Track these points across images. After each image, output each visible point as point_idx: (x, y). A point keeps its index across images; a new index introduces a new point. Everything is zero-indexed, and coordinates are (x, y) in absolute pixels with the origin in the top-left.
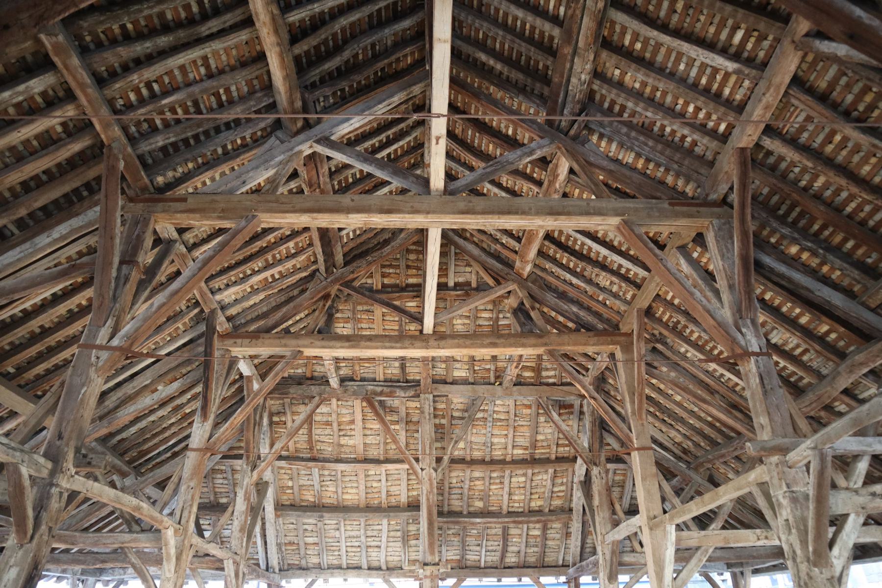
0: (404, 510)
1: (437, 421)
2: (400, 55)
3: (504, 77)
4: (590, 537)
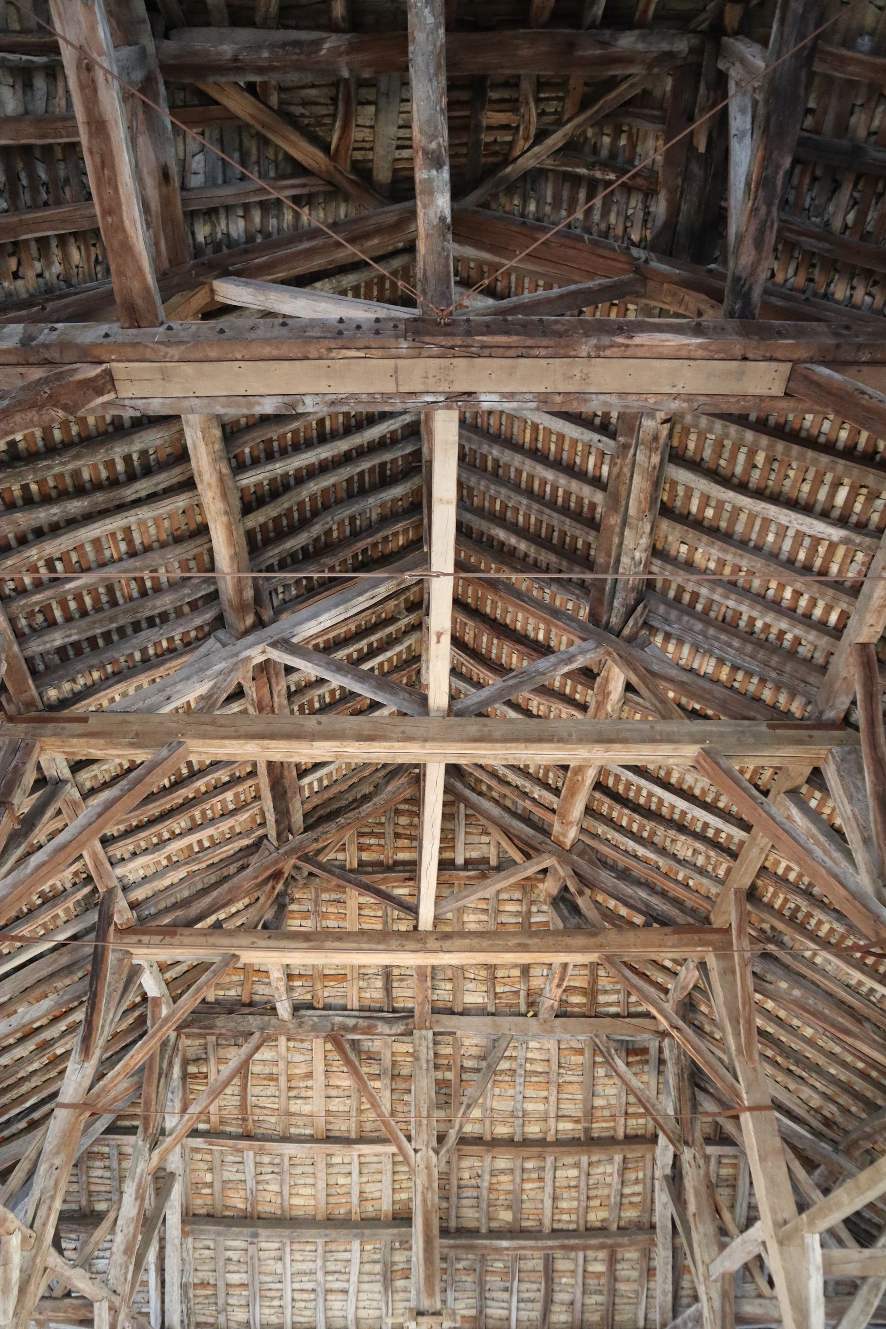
0: (387, 1226)
1: (440, 1075)
2: (388, 532)
3: (531, 560)
4: (686, 1277)
